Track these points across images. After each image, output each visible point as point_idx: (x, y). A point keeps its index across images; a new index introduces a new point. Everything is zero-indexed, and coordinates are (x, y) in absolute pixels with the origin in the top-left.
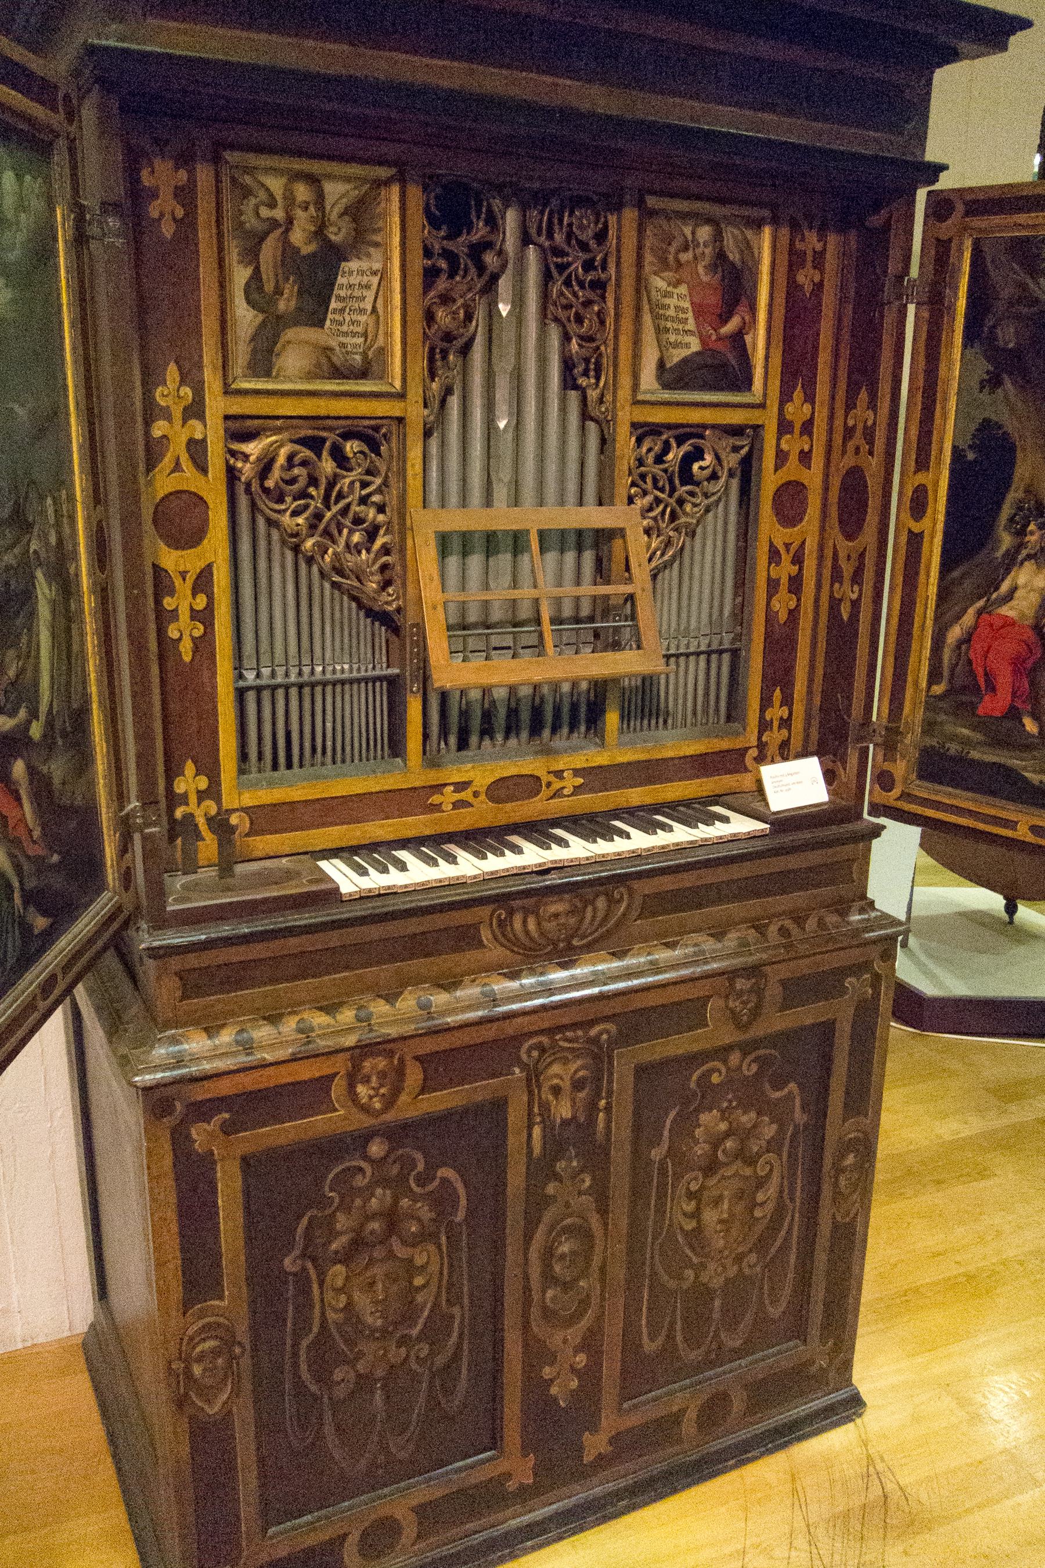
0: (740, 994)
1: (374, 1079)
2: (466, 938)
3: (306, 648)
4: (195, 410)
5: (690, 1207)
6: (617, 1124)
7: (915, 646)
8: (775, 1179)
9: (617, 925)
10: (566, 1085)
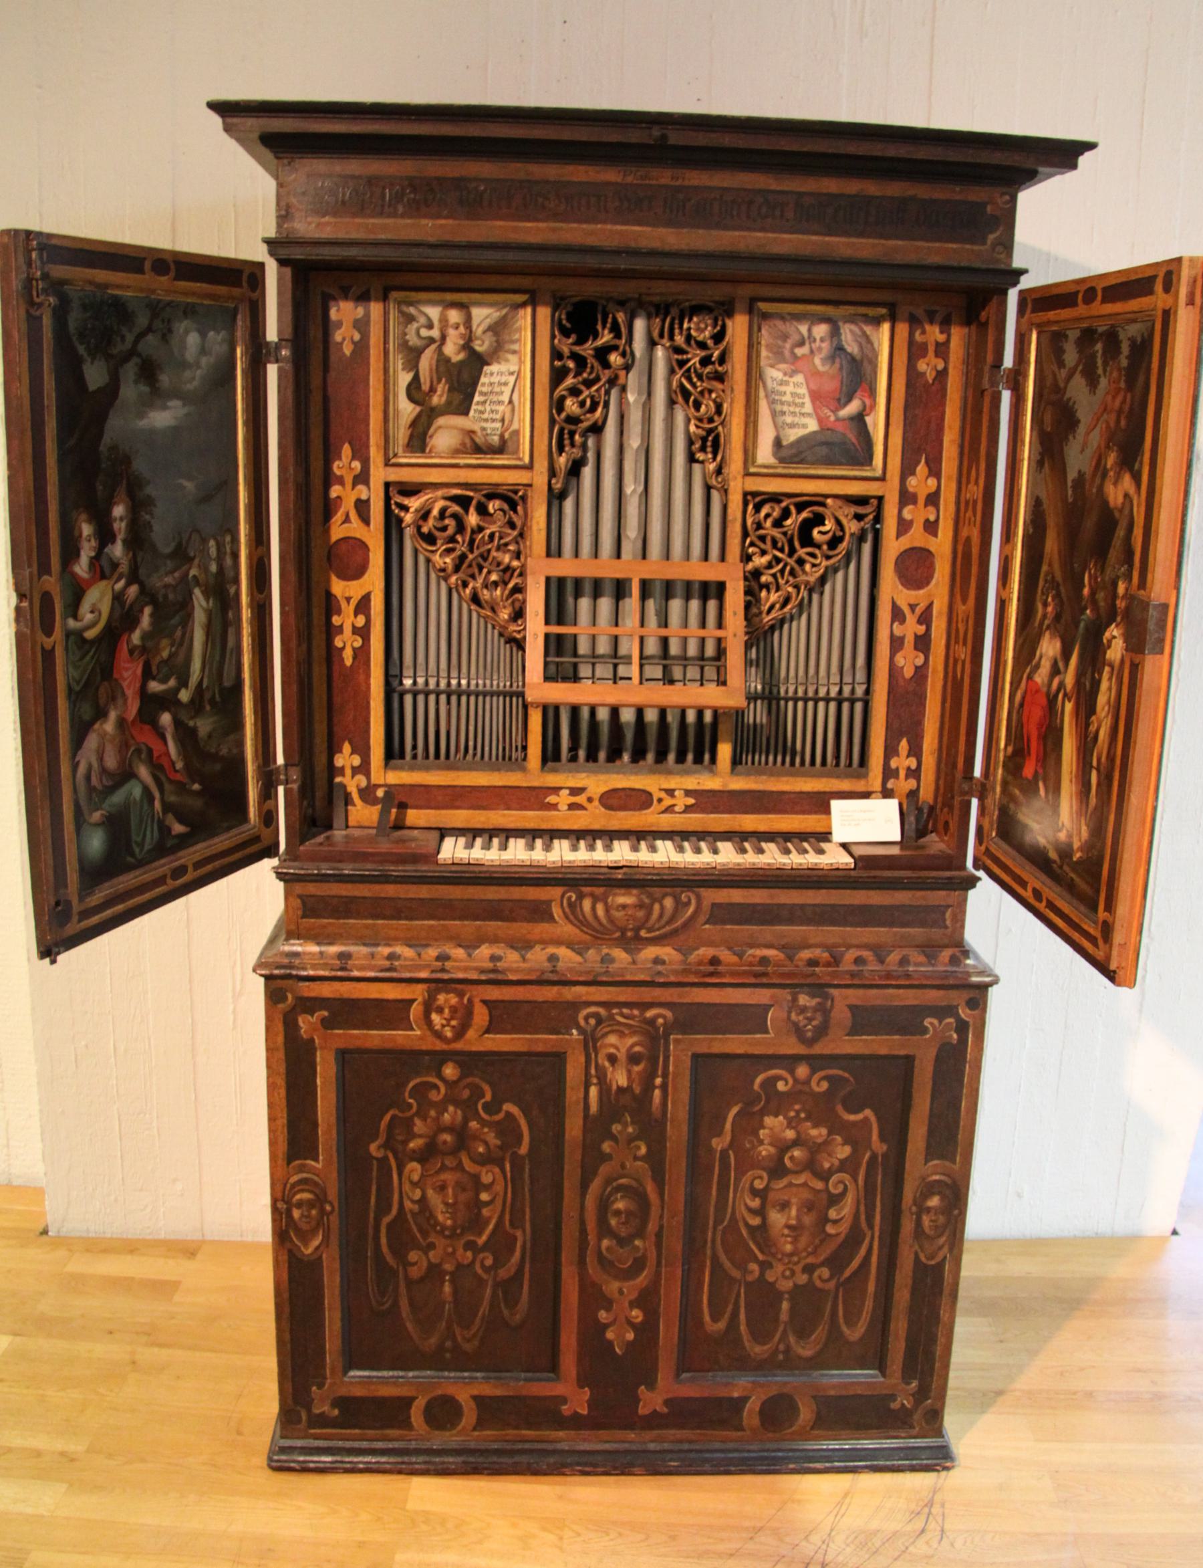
0: (803, 1010)
1: (447, 1011)
3: (454, 661)
4: (363, 478)
5: (755, 1203)
6: (675, 1103)
8: (850, 1199)
9: (685, 925)
10: (622, 1055)
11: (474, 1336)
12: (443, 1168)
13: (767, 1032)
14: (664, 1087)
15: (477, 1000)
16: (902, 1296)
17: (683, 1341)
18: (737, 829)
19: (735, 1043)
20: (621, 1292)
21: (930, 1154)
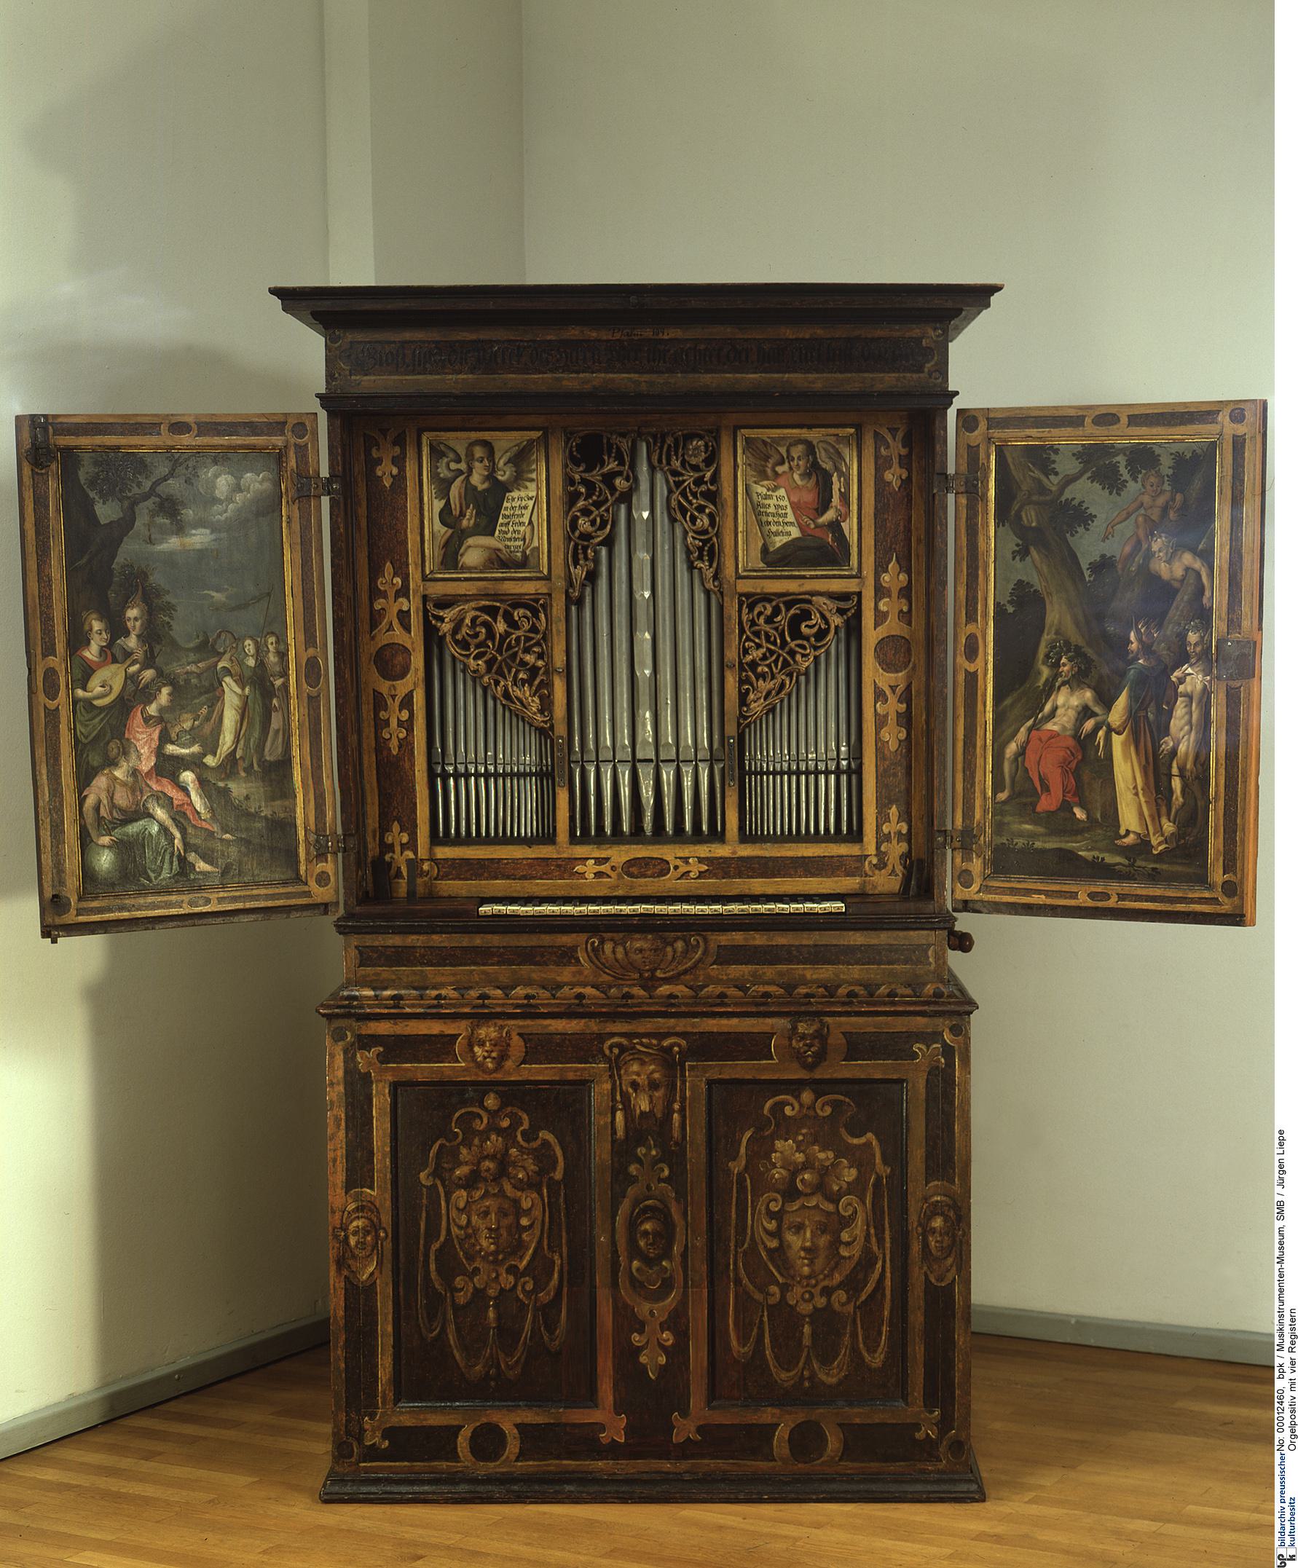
0: (803, 1037)
4: (404, 592)
5: (772, 1226)
6: (690, 1126)
7: (979, 761)
10: (642, 1080)
11: (517, 1362)
13: (772, 1059)
14: (682, 1110)
16: (917, 1319)
17: (712, 1363)
18: (747, 892)
20: (651, 1313)
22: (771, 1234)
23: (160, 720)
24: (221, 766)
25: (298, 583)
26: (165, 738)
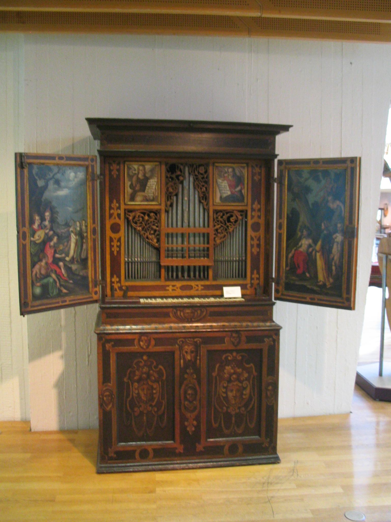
0: (234, 337)
2: (167, 315)
4: (119, 208)
5: (224, 390)
6: (203, 364)
10: (189, 351)
12: (144, 384)
14: (200, 359)
15: (152, 339)
16: (264, 414)
19: (217, 347)
20: (190, 416)
21: (268, 375)
22: (224, 392)
23: (54, 246)
24: (70, 260)
25: (91, 205)
26: (55, 252)
